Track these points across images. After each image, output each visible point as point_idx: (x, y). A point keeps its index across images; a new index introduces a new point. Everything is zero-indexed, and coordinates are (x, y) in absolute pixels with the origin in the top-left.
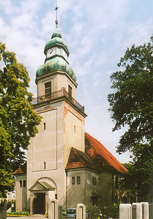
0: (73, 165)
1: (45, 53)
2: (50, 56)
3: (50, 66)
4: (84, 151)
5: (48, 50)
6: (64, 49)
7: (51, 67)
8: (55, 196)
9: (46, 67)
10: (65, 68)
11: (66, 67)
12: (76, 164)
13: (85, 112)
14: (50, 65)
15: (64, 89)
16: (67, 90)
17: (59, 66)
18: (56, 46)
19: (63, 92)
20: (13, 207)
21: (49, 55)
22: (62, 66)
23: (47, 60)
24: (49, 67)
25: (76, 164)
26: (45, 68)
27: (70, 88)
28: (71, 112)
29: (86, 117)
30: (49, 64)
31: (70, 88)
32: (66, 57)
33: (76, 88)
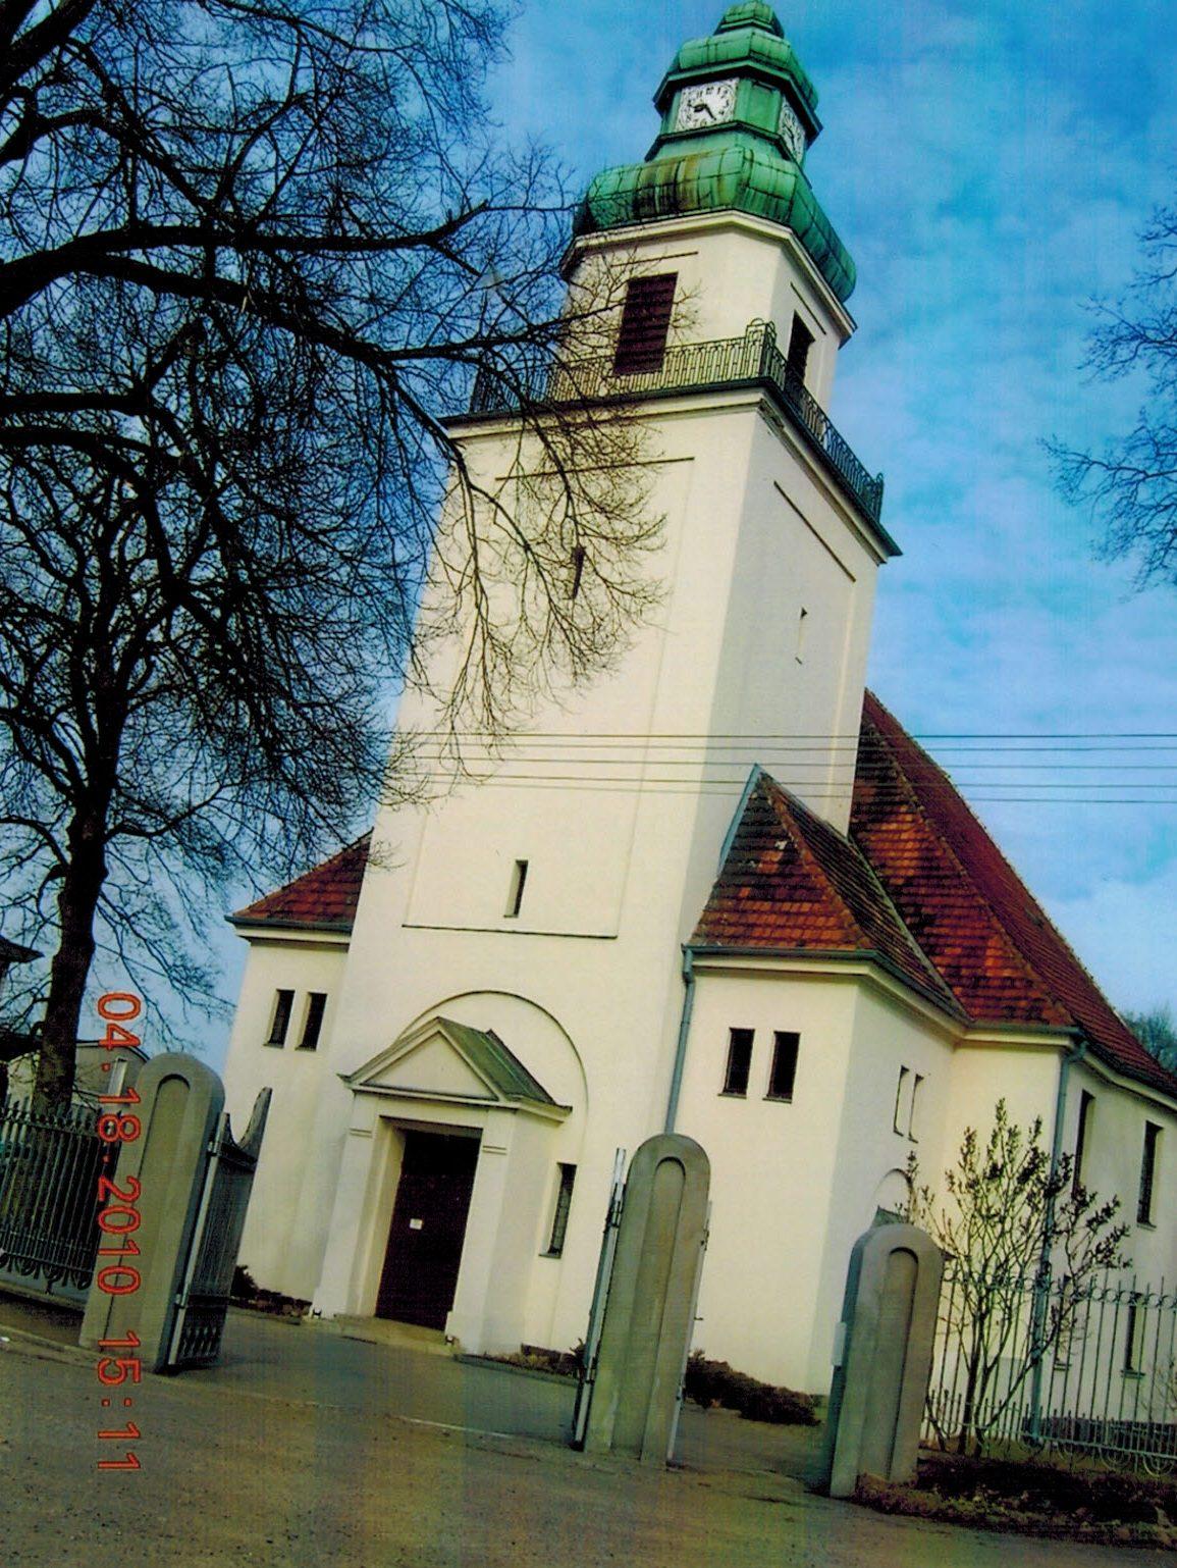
0: (752, 919)
1: (664, 103)
2: (691, 125)
3: (686, 181)
4: (845, 832)
5: (687, 91)
6: (788, 100)
7: (693, 185)
8: (569, 1104)
9: (660, 180)
10: (784, 204)
11: (792, 202)
12: (781, 921)
13: (889, 522)
14: (686, 172)
15: (767, 335)
16: (783, 345)
17: (747, 185)
18: (785, 89)
19: (756, 352)
20: (155, 561)
21: (685, 118)
22: (770, 190)
23: (662, 141)
24: (675, 183)
25: (781, 921)
26: (651, 186)
27: (802, 337)
28: (1112, 733)
29: (891, 560)
30: (683, 165)
31: (802, 337)
32: (796, 145)
33: (840, 347)
